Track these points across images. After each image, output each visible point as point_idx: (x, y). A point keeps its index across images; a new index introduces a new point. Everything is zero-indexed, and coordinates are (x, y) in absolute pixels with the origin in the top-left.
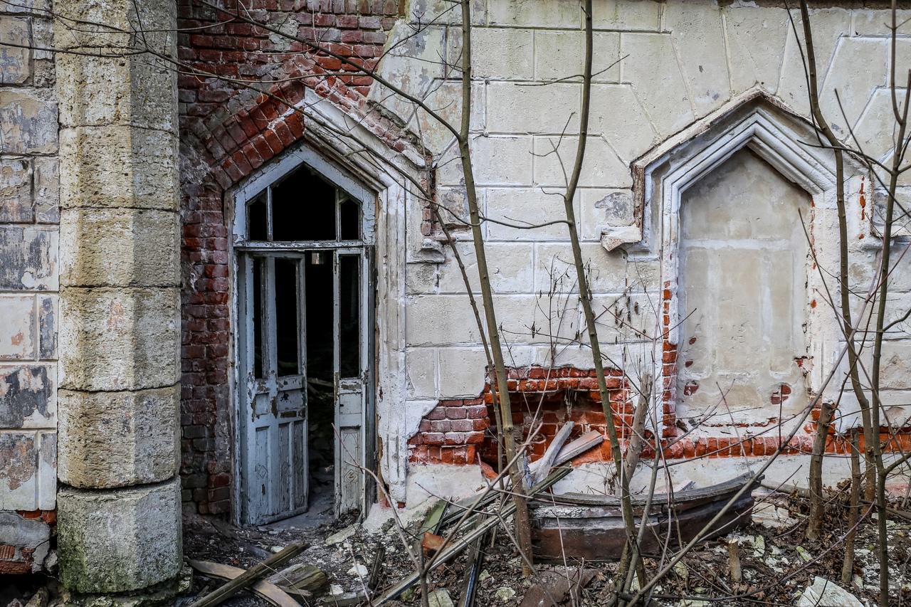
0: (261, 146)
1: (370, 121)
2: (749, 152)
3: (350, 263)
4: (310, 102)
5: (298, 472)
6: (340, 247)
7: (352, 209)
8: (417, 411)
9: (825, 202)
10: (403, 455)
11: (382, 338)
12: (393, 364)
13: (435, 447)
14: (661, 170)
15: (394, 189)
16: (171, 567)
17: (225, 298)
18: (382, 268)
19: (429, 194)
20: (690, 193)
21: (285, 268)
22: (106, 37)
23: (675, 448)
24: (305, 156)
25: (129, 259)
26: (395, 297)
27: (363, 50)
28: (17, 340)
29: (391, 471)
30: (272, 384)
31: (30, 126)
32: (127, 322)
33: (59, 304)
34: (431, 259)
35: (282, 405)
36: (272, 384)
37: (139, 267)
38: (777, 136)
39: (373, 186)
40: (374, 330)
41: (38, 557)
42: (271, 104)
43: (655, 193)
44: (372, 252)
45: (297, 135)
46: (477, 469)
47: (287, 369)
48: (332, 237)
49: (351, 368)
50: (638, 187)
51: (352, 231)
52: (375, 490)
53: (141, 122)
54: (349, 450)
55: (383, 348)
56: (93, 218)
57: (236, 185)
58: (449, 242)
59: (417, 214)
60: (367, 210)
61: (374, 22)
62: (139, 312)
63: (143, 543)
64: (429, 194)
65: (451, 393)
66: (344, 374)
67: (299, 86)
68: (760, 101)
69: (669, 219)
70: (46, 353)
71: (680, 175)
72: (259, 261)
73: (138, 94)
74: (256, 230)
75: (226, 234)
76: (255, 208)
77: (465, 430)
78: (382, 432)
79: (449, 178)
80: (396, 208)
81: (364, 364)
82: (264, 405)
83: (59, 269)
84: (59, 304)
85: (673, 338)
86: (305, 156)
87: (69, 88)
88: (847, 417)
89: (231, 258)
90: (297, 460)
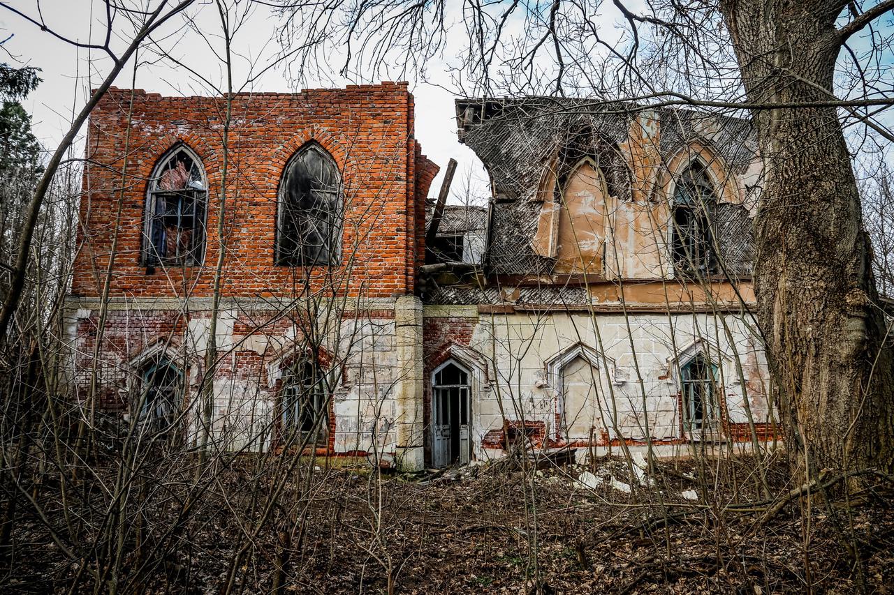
0: (439, 359)
1: (470, 352)
2: (578, 357)
3: (464, 391)
4: (453, 347)
5: (448, 454)
6: (461, 387)
7: (465, 376)
8: (483, 433)
9: (603, 371)
10: (480, 446)
11: (473, 413)
12: (477, 420)
13: (489, 444)
14: (552, 364)
15: (477, 370)
16: (422, 468)
17: (430, 401)
18: (473, 393)
19: (486, 374)
20: (562, 370)
21: (445, 392)
22: (409, 340)
23: (559, 444)
24: (452, 361)
25: (414, 391)
26: (477, 401)
27: (467, 332)
28: (387, 411)
29: (476, 451)
30: (441, 427)
31: (390, 360)
32: (413, 407)
33: (397, 402)
34: (487, 390)
35: (444, 433)
36: (441, 427)
37: (416, 393)
38: (589, 354)
39: (470, 369)
40: (471, 410)
41: (391, 464)
42: (444, 347)
43: (551, 370)
44: (470, 388)
45: (450, 355)
46: (500, 451)
47: (445, 422)
48: (458, 383)
49: (464, 422)
50: (546, 368)
51: (464, 382)
52: (472, 456)
53: (416, 359)
54: (464, 446)
55: (474, 416)
56: (406, 382)
57: (433, 370)
58: (492, 385)
59: (483, 378)
60: (469, 376)
61: (470, 325)
62: (416, 404)
63: (417, 461)
64: (486, 374)
65: (494, 428)
66: (462, 424)
67: (450, 343)
68: (580, 344)
69: (556, 378)
70: (393, 414)
71: (558, 365)
72: (438, 390)
73: (416, 353)
74: (438, 383)
75: (430, 383)
76: (438, 376)
77: (497, 439)
78: (473, 439)
79: (491, 369)
80: (477, 376)
81: (468, 420)
82: (439, 433)
83: (397, 394)
84: (397, 402)
85: (558, 412)
86: (452, 361)
87: (400, 352)
88: (612, 434)
89: (431, 390)
90: (448, 450)
